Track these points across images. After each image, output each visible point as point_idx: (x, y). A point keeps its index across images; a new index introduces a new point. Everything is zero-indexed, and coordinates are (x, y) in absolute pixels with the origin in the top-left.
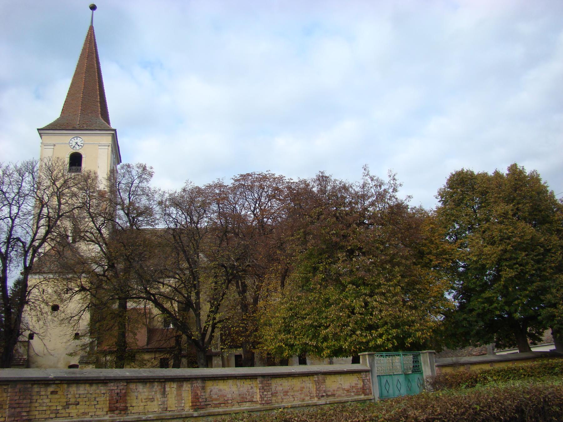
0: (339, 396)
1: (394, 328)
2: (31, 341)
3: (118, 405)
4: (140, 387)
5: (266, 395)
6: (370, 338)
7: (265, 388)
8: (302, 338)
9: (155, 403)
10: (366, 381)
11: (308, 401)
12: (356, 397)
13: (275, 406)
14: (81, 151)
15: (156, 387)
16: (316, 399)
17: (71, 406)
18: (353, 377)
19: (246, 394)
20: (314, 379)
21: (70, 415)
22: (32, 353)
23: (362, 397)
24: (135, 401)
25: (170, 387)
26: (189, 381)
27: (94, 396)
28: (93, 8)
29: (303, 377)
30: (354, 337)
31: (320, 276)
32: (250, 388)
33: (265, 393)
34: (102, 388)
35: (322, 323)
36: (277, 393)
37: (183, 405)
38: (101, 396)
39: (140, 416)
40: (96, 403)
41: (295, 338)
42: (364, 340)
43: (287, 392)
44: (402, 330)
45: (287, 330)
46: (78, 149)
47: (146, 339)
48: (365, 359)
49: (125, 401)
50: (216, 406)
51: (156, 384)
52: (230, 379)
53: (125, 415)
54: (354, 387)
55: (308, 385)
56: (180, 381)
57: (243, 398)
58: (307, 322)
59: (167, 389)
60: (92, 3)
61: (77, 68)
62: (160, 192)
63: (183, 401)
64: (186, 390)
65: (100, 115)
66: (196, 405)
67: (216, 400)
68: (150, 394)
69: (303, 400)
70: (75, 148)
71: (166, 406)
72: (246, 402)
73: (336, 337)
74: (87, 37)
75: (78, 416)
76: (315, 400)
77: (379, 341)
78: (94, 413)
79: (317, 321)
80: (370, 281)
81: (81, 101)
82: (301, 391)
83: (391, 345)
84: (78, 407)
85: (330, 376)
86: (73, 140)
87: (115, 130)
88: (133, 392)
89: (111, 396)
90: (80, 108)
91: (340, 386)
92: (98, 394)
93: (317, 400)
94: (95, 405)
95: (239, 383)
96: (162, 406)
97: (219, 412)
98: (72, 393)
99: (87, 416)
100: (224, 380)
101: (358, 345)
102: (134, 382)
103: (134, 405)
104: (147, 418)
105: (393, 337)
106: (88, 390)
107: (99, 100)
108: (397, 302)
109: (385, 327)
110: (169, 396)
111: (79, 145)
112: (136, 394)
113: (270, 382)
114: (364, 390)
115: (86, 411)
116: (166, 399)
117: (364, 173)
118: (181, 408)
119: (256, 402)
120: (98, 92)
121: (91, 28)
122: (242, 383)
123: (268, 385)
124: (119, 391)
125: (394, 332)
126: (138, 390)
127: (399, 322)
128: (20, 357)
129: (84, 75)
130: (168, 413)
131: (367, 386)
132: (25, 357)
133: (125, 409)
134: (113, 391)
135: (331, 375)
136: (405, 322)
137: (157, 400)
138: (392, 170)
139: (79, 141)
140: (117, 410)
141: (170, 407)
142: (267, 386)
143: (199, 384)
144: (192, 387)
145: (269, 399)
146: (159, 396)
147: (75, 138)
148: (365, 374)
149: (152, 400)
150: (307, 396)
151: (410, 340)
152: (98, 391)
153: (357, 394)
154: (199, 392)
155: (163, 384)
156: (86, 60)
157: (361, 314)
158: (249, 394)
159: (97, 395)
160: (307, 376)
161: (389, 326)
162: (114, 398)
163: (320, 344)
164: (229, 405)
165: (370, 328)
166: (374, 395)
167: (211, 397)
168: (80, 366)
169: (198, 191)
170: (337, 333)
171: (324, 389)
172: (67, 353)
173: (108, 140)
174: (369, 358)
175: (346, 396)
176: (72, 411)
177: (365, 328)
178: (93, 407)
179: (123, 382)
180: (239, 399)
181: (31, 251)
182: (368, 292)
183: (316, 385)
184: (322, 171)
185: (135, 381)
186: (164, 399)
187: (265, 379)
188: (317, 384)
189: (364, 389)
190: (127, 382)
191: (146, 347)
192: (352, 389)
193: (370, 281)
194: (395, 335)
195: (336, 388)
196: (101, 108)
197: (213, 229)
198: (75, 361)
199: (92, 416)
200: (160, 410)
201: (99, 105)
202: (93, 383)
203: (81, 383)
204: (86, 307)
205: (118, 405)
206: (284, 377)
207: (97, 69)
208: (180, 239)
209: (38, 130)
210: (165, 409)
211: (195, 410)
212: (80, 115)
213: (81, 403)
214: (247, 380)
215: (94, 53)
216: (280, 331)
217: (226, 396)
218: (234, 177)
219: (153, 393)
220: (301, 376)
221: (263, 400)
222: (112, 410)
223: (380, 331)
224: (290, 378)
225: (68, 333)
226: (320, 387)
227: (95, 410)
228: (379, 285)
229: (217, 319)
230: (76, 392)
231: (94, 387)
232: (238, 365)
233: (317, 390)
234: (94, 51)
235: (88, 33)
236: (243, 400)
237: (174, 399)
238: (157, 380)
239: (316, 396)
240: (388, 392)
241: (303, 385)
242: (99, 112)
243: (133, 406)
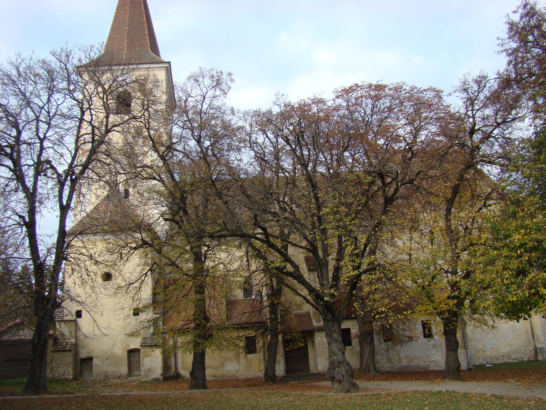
2: (78, 319)
65: (150, 49)
90: (126, 41)
107: (147, 33)
120: (146, 25)
128: (66, 341)
132: (73, 340)
168: (142, 350)
181: (68, 183)
196: (150, 42)
201: (148, 38)
204: (148, 270)
225: (126, 306)
229: (364, 267)
242: (149, 46)
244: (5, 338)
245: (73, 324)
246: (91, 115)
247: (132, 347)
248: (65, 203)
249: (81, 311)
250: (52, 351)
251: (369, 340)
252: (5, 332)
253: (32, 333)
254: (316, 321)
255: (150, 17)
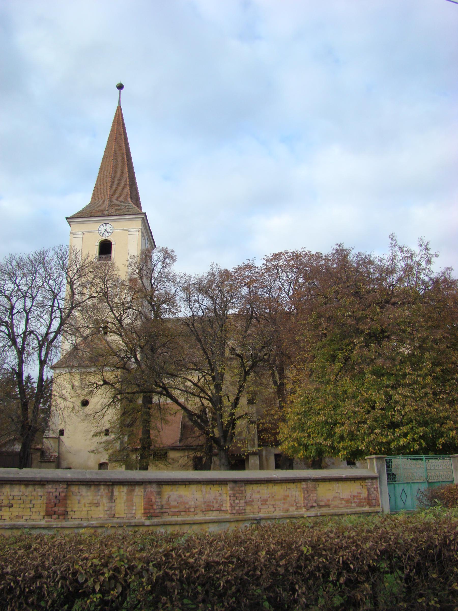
0: (335, 507)
1: (420, 427)
2: (61, 437)
3: (56, 509)
4: (84, 490)
5: (237, 503)
6: (391, 438)
7: (237, 495)
8: (316, 437)
9: (101, 508)
10: (372, 489)
11: (293, 512)
12: (358, 509)
13: (248, 516)
14: (111, 238)
15: (102, 490)
16: (304, 510)
17: (3, 509)
18: (355, 484)
19: (213, 502)
20: (302, 486)
21: (2, 518)
22: (63, 449)
23: (367, 509)
24: (77, 505)
25: (119, 492)
26: (142, 485)
27: (30, 498)
28: (120, 87)
29: (288, 484)
30: (373, 436)
31: (339, 365)
32: (218, 495)
33: (237, 501)
34: (39, 490)
35: (337, 420)
36: (253, 501)
37: (134, 512)
38: (38, 499)
39: (82, 522)
40: (31, 506)
41: (309, 436)
42: (384, 440)
43: (266, 501)
44: (432, 428)
45: (302, 427)
46: (107, 237)
47: (179, 436)
48: (372, 464)
49: (65, 506)
50: (174, 514)
51: (102, 487)
52: (194, 484)
53: (64, 520)
54: (357, 496)
55: (294, 493)
56: (131, 485)
57: (208, 506)
58: (321, 418)
59: (116, 493)
60: (119, 82)
61: (105, 152)
62: (186, 277)
63: (134, 508)
64: (137, 495)
65: (130, 199)
66: (149, 513)
67: (175, 507)
68: (95, 498)
69: (287, 510)
70: (104, 236)
71: (113, 512)
72: (213, 511)
73: (352, 436)
74: (115, 118)
75: (11, 519)
76: (303, 511)
77: (402, 442)
78: (29, 517)
79: (331, 417)
80: (393, 370)
81: (110, 185)
82: (284, 499)
83: (418, 447)
84: (11, 509)
85: (323, 483)
86: (102, 227)
87: (145, 214)
88: (75, 496)
89: (49, 499)
90: (109, 193)
91: (337, 495)
92: (35, 496)
93: (305, 511)
94: (30, 508)
95: (204, 488)
96: (108, 512)
97: (177, 521)
98: (5, 494)
99: (21, 520)
100: (185, 485)
101: (377, 446)
102: (76, 485)
103: (75, 509)
104: (89, 524)
105: (421, 437)
106: (23, 492)
107: (128, 183)
108: (426, 394)
109: (410, 425)
110: (117, 501)
111: (108, 232)
112: (78, 497)
113: (243, 488)
114: (369, 501)
115: (21, 514)
116: (113, 504)
117: (392, 244)
118: (132, 515)
119: (226, 511)
120: (127, 175)
121: (119, 109)
122: (209, 489)
123: (240, 492)
124: (58, 494)
125: (421, 430)
126: (81, 493)
127: (427, 419)
129: (112, 158)
130: (115, 520)
131: (373, 495)
132: (57, 454)
133: (65, 514)
134: (51, 494)
135: (325, 481)
136: (435, 419)
137: (103, 505)
138: (423, 238)
139: (108, 227)
140: (55, 514)
141: (118, 513)
142: (239, 493)
143: (154, 488)
144: (145, 491)
145: (241, 508)
146: (105, 500)
147: (104, 225)
148: (370, 481)
149: (97, 505)
150: (292, 505)
151: (442, 440)
152: (34, 493)
153: (360, 505)
154: (153, 498)
155: (111, 488)
156: (114, 143)
157: (382, 409)
158: (217, 502)
159: (33, 498)
160: (294, 483)
161: (414, 424)
162: (52, 501)
163: (335, 444)
164: (191, 513)
165: (394, 426)
166: (382, 508)
167: (169, 504)
169: (226, 275)
170: (353, 432)
171: (315, 498)
172: (90, 450)
173: (137, 224)
174: (376, 462)
175: (345, 507)
176: (5, 514)
177: (387, 425)
178: (29, 510)
179: (63, 484)
180: (203, 507)
182: (391, 383)
183: (304, 494)
184: (339, 243)
185: (77, 483)
186: (111, 504)
187: (237, 485)
188: (306, 492)
189: (369, 500)
190: (67, 485)
191: (178, 444)
192: (353, 499)
193: (393, 370)
194: (421, 434)
195: (331, 498)
196: (130, 192)
197: (239, 316)
198: (104, 458)
199: (26, 520)
200: (106, 516)
201: (128, 188)
202: (29, 484)
203: (16, 484)
205: (56, 509)
206: (263, 483)
207: (126, 150)
208: (194, 327)
209: (67, 218)
210: (113, 515)
211: (148, 518)
212: (108, 200)
213: (15, 506)
214: (215, 486)
215: (123, 134)
216: (294, 428)
217: (187, 503)
218: (265, 257)
219: (99, 497)
220: (285, 483)
221: (234, 509)
222: (48, 514)
223: (404, 429)
224: (270, 485)
226: (309, 496)
227: (30, 513)
228: (404, 376)
230: (9, 494)
231: (30, 488)
232: (278, 466)
233: (305, 498)
234: (122, 132)
235: (116, 114)
236: (209, 508)
237: (123, 504)
238: (103, 483)
239: (304, 506)
240: (404, 503)
241: (288, 493)
242: (129, 196)
243: (75, 511)
244: (4, 449)
245: (57, 440)
246: (59, 303)
247: (102, 461)
248: (43, 358)
249: (63, 430)
250: (40, 461)
251: (288, 465)
252: (5, 444)
253: (20, 447)
254: (251, 447)
255: (132, 165)
